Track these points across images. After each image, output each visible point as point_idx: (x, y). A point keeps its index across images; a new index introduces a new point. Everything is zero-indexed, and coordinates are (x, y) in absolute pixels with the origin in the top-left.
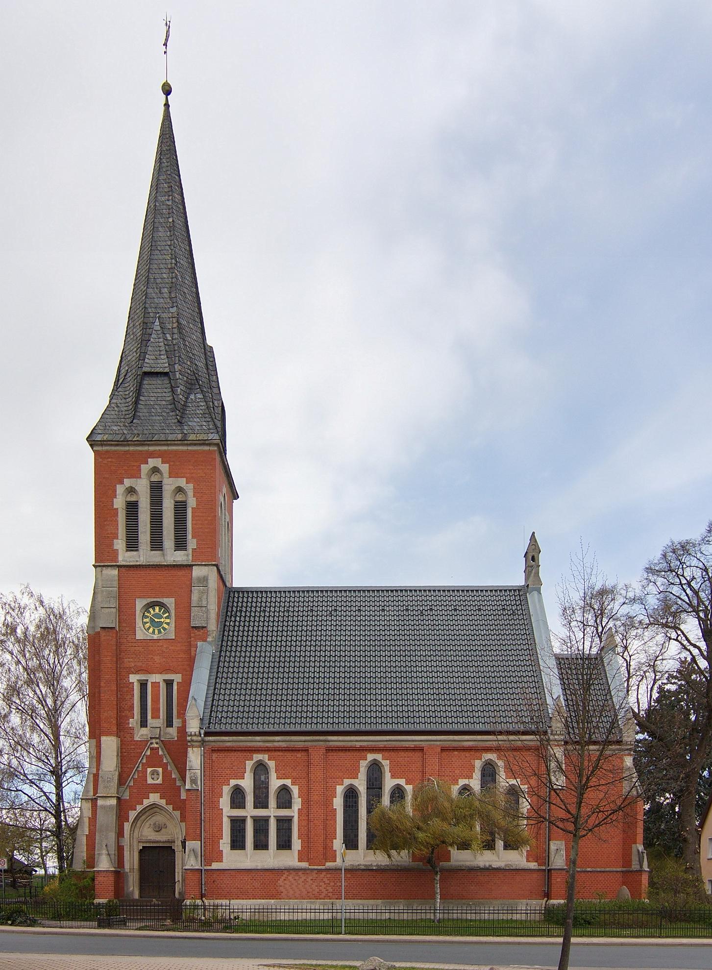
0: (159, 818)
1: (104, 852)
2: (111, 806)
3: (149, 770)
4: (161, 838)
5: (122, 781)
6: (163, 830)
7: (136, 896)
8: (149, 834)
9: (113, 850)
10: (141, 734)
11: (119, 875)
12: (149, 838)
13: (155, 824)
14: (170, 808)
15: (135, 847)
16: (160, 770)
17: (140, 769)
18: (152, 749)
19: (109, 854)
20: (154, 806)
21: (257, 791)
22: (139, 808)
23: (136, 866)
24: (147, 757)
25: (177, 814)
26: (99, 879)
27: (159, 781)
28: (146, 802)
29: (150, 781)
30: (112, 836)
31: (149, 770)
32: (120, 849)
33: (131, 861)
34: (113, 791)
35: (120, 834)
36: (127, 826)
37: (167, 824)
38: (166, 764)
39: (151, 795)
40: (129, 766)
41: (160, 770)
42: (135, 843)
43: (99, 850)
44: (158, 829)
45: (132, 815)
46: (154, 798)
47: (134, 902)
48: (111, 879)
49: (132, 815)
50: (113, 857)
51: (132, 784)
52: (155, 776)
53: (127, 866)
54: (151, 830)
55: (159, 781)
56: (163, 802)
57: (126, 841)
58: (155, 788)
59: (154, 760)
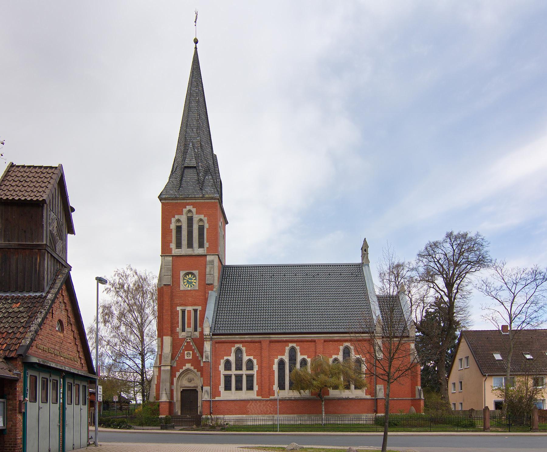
0: (190, 376)
1: (164, 392)
2: (167, 370)
3: (186, 352)
4: (191, 385)
5: (173, 358)
7: (179, 414)
8: (185, 383)
16: (191, 352)
18: (187, 342)
20: (188, 370)
22: (181, 371)
23: (179, 399)
25: (199, 373)
26: (162, 406)
27: (191, 358)
28: (184, 368)
30: (168, 384)
31: (186, 352)
32: (172, 391)
33: (177, 396)
35: (172, 383)
36: (175, 380)
41: (191, 352)
42: (179, 388)
45: (178, 374)
46: (188, 366)
49: (178, 374)
52: (189, 355)
53: (175, 399)
55: (191, 358)
56: (192, 368)
57: (174, 387)
58: (188, 361)
59: (188, 348)
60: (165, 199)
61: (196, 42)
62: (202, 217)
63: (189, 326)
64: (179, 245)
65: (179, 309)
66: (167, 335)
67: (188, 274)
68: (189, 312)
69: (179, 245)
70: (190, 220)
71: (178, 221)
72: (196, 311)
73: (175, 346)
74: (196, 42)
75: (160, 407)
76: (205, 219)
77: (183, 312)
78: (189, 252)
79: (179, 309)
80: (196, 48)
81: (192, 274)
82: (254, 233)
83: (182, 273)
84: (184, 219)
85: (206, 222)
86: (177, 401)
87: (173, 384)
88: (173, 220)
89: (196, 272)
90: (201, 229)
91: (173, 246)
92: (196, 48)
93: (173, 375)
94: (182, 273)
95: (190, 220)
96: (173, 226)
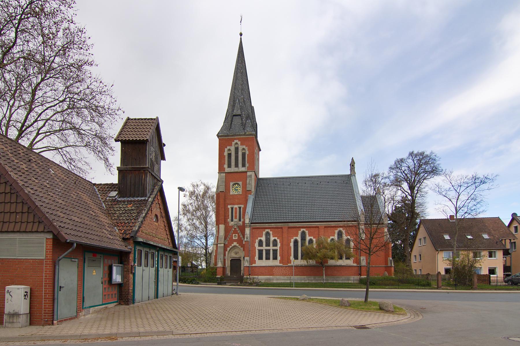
0: (236, 250)
4: (237, 256)
8: (233, 255)
9: (222, 260)
11: (224, 268)
20: (235, 246)
22: (231, 247)
26: (218, 269)
28: (233, 245)
30: (222, 255)
32: (225, 260)
33: (228, 264)
35: (225, 255)
36: (227, 253)
44: (236, 253)
45: (228, 249)
49: (228, 249)
53: (226, 265)
56: (238, 245)
57: (226, 257)
58: (235, 241)
59: (235, 232)
60: (221, 136)
61: (241, 34)
62: (244, 147)
63: (236, 218)
64: (229, 166)
65: (229, 207)
67: (235, 184)
68: (236, 208)
69: (229, 166)
70: (237, 149)
71: (229, 150)
72: (240, 208)
74: (241, 34)
76: (246, 148)
77: (232, 208)
78: (236, 170)
79: (229, 207)
80: (241, 39)
81: (238, 184)
83: (231, 184)
84: (233, 148)
85: (247, 150)
88: (226, 150)
89: (240, 183)
90: (244, 155)
91: (226, 166)
92: (241, 39)
94: (231, 184)
95: (237, 149)
96: (226, 154)
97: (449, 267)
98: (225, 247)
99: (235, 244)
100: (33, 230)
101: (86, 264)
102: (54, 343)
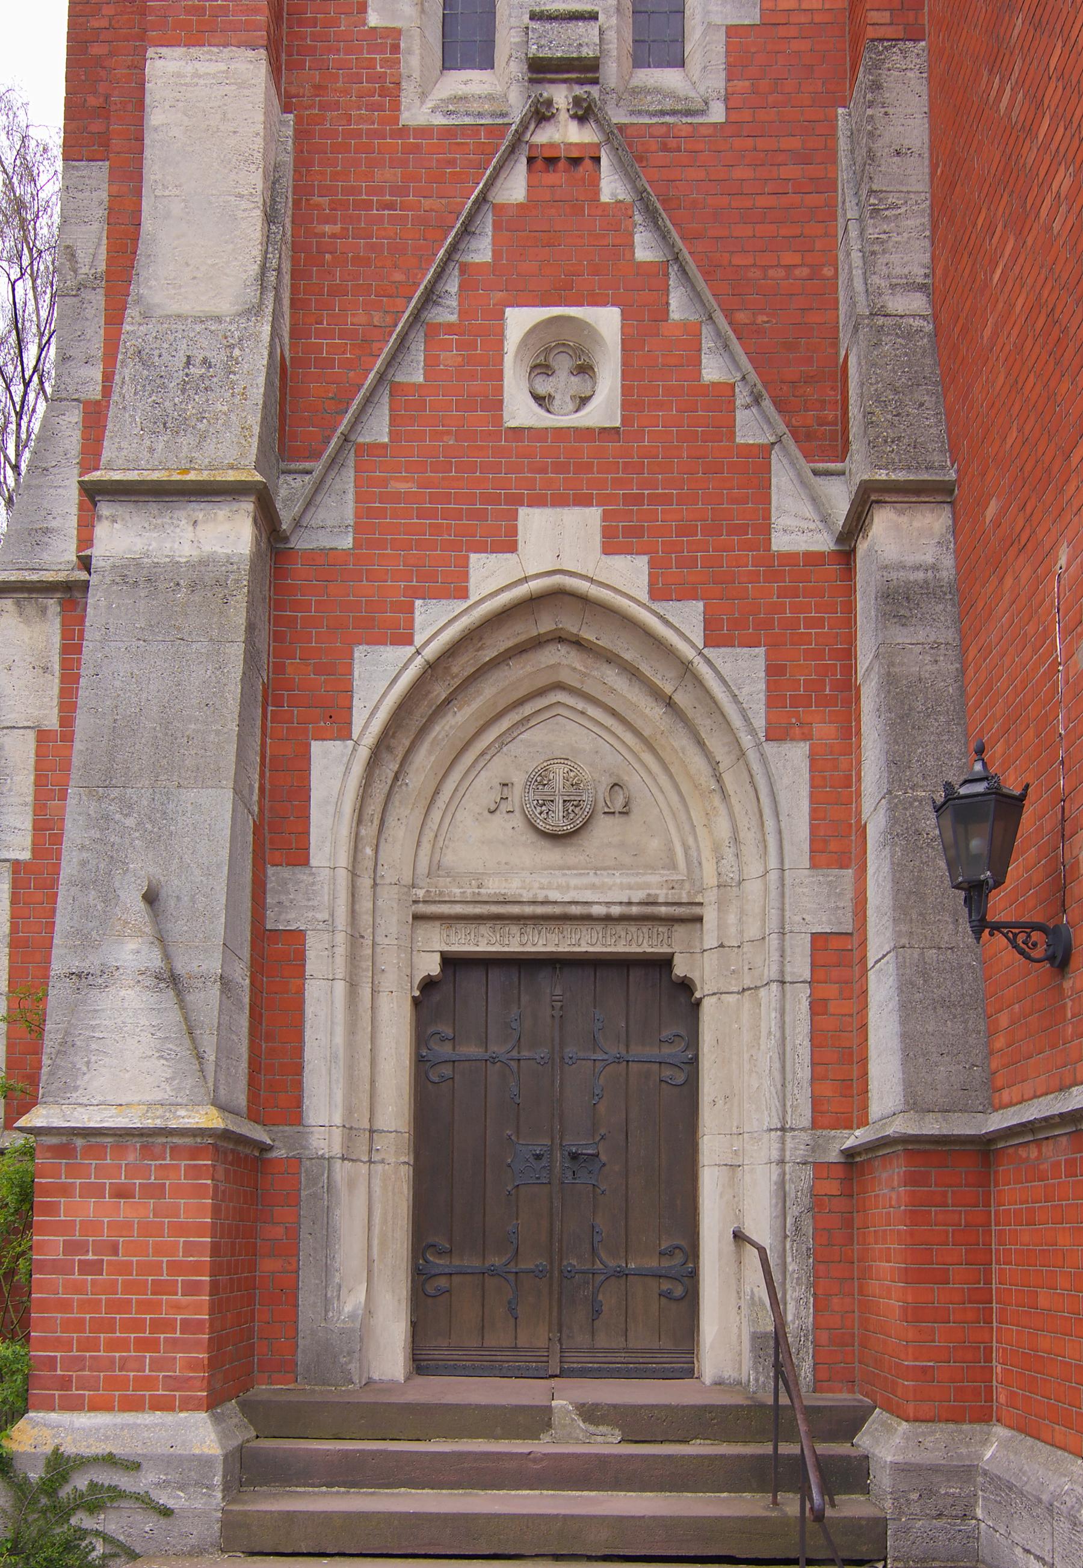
0: (570, 741)
1: (133, 953)
2: (203, 578)
3: (520, 321)
4: (596, 882)
5: (298, 419)
6: (605, 830)
7: (389, 1356)
8: (494, 861)
9: (210, 951)
10: (435, 97)
11: (252, 1180)
12: (494, 887)
13: (540, 780)
14: (684, 623)
15: (391, 961)
16: (606, 321)
17: (447, 313)
18: (545, 161)
19: (172, 980)
20: (554, 614)
21: (191, 1407)
22: (436, 623)
23: (394, 1110)
24: (510, 221)
25: (741, 675)
26: (80, 1214)
27: (604, 408)
28: (491, 579)
29: (520, 410)
30: (210, 818)
31: (520, 321)
32: (273, 965)
33: (357, 1075)
34: (231, 445)
35: (276, 831)
36: (333, 772)
37: (634, 781)
38: (654, 279)
39: (535, 524)
40: (357, 318)
41: (606, 321)
42: (392, 922)
43: (85, 942)
44: (563, 822)
45: (379, 678)
46: (558, 542)
47: (384, 1417)
48: (186, 1214)
49: (379, 678)
50: (207, 1001)
51: (378, 429)
52: (562, 384)
53: (324, 1106)
54: (508, 826)
55: (604, 408)
56: (627, 578)
57: (319, 897)
58: (563, 468)
59: (562, 256)
66: (200, 31)
73: (344, 230)
75: (48, 1245)
82: (919, 273)
86: (361, 1136)
87: (300, 857)
93: (288, 697)
97: (285, 872)
98: (294, 630)
99: (558, 542)
100: (1025, 1097)
101: (631, 978)
102: (889, 966)
